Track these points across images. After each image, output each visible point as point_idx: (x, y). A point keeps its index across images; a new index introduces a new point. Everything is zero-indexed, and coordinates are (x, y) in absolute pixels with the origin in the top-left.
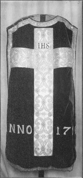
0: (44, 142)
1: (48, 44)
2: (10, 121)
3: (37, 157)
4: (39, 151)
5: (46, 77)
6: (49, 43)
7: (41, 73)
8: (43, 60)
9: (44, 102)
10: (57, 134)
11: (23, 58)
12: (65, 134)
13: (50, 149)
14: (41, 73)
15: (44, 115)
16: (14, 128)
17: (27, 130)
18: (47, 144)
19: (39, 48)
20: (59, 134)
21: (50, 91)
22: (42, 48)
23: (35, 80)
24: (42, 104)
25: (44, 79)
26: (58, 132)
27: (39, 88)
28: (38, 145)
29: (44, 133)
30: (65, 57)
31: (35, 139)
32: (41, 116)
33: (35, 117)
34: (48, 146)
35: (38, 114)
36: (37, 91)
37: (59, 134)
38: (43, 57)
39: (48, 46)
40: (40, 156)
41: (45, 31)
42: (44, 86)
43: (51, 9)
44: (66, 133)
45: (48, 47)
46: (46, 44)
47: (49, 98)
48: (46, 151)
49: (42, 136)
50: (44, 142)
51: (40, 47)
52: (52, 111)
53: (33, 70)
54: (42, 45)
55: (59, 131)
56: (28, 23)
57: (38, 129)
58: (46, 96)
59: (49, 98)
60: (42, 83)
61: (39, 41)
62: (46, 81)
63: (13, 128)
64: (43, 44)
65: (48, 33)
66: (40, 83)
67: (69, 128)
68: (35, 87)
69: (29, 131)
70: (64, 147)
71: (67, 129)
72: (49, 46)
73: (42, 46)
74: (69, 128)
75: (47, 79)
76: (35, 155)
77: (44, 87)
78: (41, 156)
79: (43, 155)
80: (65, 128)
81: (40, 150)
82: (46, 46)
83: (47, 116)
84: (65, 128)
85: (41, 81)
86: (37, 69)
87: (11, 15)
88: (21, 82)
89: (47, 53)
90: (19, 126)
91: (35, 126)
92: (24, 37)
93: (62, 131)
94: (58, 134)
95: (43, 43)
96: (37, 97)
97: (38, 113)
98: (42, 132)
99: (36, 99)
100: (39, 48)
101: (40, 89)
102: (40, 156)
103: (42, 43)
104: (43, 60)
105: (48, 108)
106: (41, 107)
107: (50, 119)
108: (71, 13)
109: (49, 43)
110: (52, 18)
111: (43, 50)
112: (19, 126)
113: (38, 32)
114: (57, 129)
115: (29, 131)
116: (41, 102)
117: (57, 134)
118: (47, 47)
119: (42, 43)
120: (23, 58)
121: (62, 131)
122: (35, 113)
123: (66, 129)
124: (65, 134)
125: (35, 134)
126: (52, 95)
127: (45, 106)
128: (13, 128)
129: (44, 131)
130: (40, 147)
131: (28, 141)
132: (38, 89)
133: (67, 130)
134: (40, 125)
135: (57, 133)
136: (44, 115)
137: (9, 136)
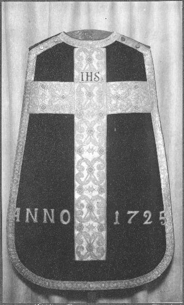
0: (90, 234)
1: (97, 74)
2: (22, 201)
3: (83, 263)
4: (83, 253)
5: (95, 128)
6: (99, 73)
7: (86, 122)
8: (90, 102)
9: (90, 170)
10: (115, 223)
11: (54, 98)
12: (130, 222)
13: (103, 249)
14: (86, 122)
15: (91, 192)
17: (69, 217)
18: (97, 239)
19: (83, 80)
20: (119, 224)
21: (100, 151)
23: (77, 133)
24: (88, 172)
25: (91, 131)
27: (83, 147)
28: (82, 242)
29: (91, 222)
30: (124, 97)
31: (76, 232)
32: (86, 193)
33: (77, 196)
34: (98, 243)
35: (81, 190)
36: (80, 152)
37: (119, 224)
38: (90, 94)
39: (97, 77)
40: (84, 260)
41: (93, 53)
42: (91, 143)
43: (99, 17)
45: (97, 79)
46: (93, 73)
47: (100, 163)
48: (95, 251)
49: (87, 227)
50: (90, 234)
51: (85, 78)
52: (104, 183)
53: (71, 117)
54: (87, 76)
56: (114, 41)
57: (80, 216)
58: (95, 160)
59: (100, 163)
60: (87, 137)
61: (82, 69)
62: (95, 135)
63: (51, 217)
64: (89, 74)
65: (97, 56)
66: (84, 139)
67: (136, 212)
68: (77, 145)
69: (66, 219)
70: (135, 244)
72: (100, 78)
74: (136, 212)
75: (96, 131)
76: (77, 258)
77: (91, 145)
78: (86, 260)
79: (89, 259)
80: (129, 212)
81: (85, 251)
82: (94, 76)
83: (96, 193)
84: (129, 212)
85: (85, 134)
86: (80, 115)
87: (55, 22)
88: (50, 138)
89: (96, 89)
90: (45, 210)
91: (77, 209)
92: (55, 63)
93: (124, 217)
94: (117, 223)
96: (79, 162)
97: (81, 189)
98: (87, 219)
99: (78, 164)
100: (83, 80)
101: (85, 148)
102: (85, 261)
103: (87, 73)
104: (90, 102)
105: (97, 178)
106: (87, 177)
107: (101, 198)
109: (99, 73)
110: (104, 35)
111: (89, 84)
112: (45, 210)
113: (80, 55)
114: (115, 216)
116: (85, 169)
117: (115, 223)
118: (95, 78)
119: (87, 73)
120: (54, 98)
122: (76, 188)
124: (130, 222)
125: (77, 222)
126: (104, 157)
127: (93, 176)
128: (51, 217)
129: (91, 218)
130: (84, 245)
131: (64, 235)
132: (82, 149)
133: (134, 216)
134: (85, 207)
135: (38, 211)
136: (91, 192)
137: (21, 228)
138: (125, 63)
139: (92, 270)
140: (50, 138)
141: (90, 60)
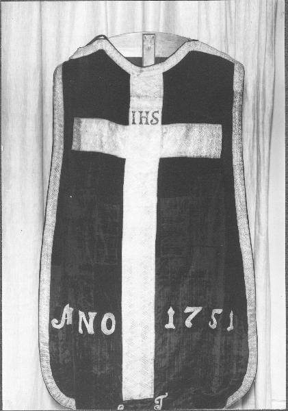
8: (144, 146)
10: (167, 326)
11: (95, 135)
12: (188, 323)
16: (81, 321)
22: (141, 123)
26: (231, 323)
44: (192, 321)
45: (155, 121)
55: (230, 323)
71: (191, 313)
73: (141, 120)
80: (188, 310)
82: (150, 118)
87: (45, 42)
93: (180, 316)
94: (170, 325)
95: (144, 110)
104: (144, 146)
108: (251, 45)
114: (167, 316)
115: (109, 326)
117: (167, 326)
118: (152, 121)
121: (180, 316)
123: (191, 313)
128: (83, 322)
141: (147, 91)
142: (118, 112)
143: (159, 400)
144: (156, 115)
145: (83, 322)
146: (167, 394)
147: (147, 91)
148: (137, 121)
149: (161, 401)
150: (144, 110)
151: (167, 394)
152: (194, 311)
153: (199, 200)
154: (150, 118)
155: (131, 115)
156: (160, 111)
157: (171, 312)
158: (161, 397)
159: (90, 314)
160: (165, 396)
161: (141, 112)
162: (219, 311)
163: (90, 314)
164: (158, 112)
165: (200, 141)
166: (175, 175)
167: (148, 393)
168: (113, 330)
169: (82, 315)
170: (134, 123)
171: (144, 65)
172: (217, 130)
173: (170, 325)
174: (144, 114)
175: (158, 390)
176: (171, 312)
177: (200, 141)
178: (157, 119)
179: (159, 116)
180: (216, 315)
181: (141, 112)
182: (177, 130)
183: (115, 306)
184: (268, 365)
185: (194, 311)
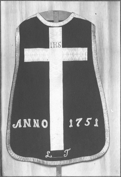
8: (56, 56)
12: (78, 125)
45: (59, 46)
71: (78, 121)
88: (31, 79)
94: (71, 126)
95: (55, 42)
104: (56, 56)
115: (45, 124)
138: (78, 33)
139: (57, 155)
140: (31, 79)
141: (56, 35)
142: (44, 43)
143: (66, 151)
144: (60, 44)
145: (37, 123)
146: (70, 149)
147: (56, 35)
148: (53, 46)
149: (67, 152)
150: (55, 42)
151: (70, 149)
152: (80, 120)
153: (81, 81)
154: (58, 45)
155: (50, 44)
156: (61, 42)
157: (71, 121)
158: (68, 150)
159: (37, 120)
160: (69, 150)
161: (54, 43)
162: (90, 119)
163: (37, 120)
164: (60, 42)
165: (80, 54)
166: (69, 67)
167: (62, 148)
168: (47, 125)
169: (29, 125)
170: (51, 47)
171: (61, 28)
172: (86, 50)
173: (71, 126)
174: (55, 44)
175: (66, 147)
176: (71, 121)
177: (80, 54)
178: (60, 45)
179: (61, 44)
180: (89, 120)
181: (54, 43)
182: (67, 50)
183: (47, 117)
184: (111, 20)
185: (80, 120)
